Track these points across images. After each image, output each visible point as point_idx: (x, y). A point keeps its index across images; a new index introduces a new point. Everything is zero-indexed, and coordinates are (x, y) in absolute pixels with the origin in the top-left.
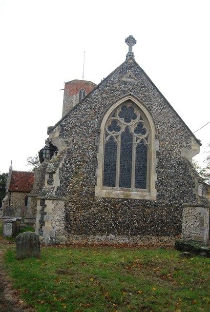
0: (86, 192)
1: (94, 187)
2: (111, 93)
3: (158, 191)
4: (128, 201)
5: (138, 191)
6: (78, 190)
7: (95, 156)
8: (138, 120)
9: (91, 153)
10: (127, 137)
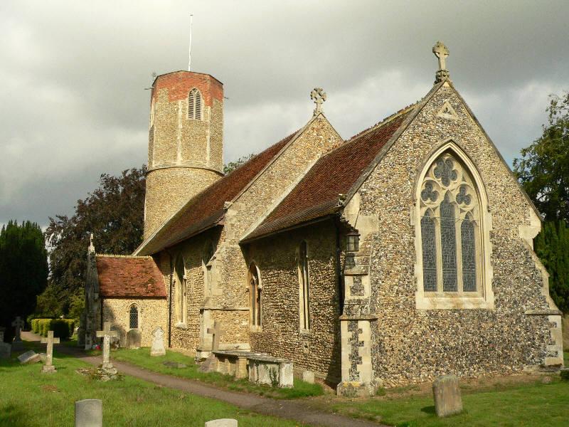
0: (404, 304)
1: (414, 295)
2: (425, 137)
3: (495, 293)
4: (458, 313)
5: (468, 296)
6: (392, 300)
7: (411, 243)
8: (459, 181)
9: (407, 237)
10: (447, 208)
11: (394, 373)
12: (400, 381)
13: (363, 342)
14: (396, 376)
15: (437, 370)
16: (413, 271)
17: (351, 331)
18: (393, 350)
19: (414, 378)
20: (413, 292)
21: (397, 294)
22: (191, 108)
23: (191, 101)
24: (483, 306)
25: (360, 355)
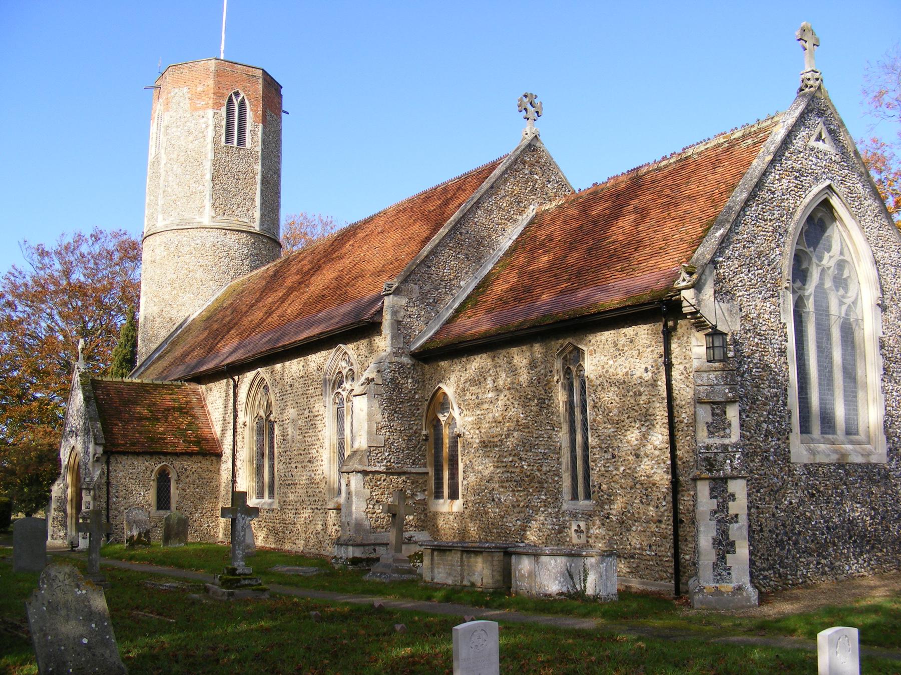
0: (775, 453)
1: (788, 438)
3: (888, 439)
11: (764, 569)
12: (772, 583)
13: (736, 516)
14: (766, 573)
15: (818, 563)
16: (786, 398)
17: (715, 497)
18: (761, 530)
19: (789, 577)
20: (785, 434)
21: (766, 436)
22: (229, 124)
23: (230, 112)
24: (874, 459)
25: (731, 538)
